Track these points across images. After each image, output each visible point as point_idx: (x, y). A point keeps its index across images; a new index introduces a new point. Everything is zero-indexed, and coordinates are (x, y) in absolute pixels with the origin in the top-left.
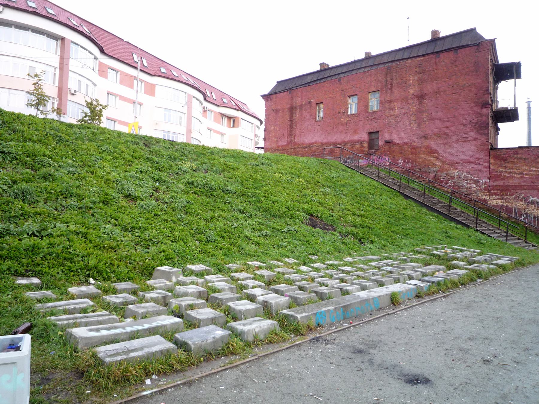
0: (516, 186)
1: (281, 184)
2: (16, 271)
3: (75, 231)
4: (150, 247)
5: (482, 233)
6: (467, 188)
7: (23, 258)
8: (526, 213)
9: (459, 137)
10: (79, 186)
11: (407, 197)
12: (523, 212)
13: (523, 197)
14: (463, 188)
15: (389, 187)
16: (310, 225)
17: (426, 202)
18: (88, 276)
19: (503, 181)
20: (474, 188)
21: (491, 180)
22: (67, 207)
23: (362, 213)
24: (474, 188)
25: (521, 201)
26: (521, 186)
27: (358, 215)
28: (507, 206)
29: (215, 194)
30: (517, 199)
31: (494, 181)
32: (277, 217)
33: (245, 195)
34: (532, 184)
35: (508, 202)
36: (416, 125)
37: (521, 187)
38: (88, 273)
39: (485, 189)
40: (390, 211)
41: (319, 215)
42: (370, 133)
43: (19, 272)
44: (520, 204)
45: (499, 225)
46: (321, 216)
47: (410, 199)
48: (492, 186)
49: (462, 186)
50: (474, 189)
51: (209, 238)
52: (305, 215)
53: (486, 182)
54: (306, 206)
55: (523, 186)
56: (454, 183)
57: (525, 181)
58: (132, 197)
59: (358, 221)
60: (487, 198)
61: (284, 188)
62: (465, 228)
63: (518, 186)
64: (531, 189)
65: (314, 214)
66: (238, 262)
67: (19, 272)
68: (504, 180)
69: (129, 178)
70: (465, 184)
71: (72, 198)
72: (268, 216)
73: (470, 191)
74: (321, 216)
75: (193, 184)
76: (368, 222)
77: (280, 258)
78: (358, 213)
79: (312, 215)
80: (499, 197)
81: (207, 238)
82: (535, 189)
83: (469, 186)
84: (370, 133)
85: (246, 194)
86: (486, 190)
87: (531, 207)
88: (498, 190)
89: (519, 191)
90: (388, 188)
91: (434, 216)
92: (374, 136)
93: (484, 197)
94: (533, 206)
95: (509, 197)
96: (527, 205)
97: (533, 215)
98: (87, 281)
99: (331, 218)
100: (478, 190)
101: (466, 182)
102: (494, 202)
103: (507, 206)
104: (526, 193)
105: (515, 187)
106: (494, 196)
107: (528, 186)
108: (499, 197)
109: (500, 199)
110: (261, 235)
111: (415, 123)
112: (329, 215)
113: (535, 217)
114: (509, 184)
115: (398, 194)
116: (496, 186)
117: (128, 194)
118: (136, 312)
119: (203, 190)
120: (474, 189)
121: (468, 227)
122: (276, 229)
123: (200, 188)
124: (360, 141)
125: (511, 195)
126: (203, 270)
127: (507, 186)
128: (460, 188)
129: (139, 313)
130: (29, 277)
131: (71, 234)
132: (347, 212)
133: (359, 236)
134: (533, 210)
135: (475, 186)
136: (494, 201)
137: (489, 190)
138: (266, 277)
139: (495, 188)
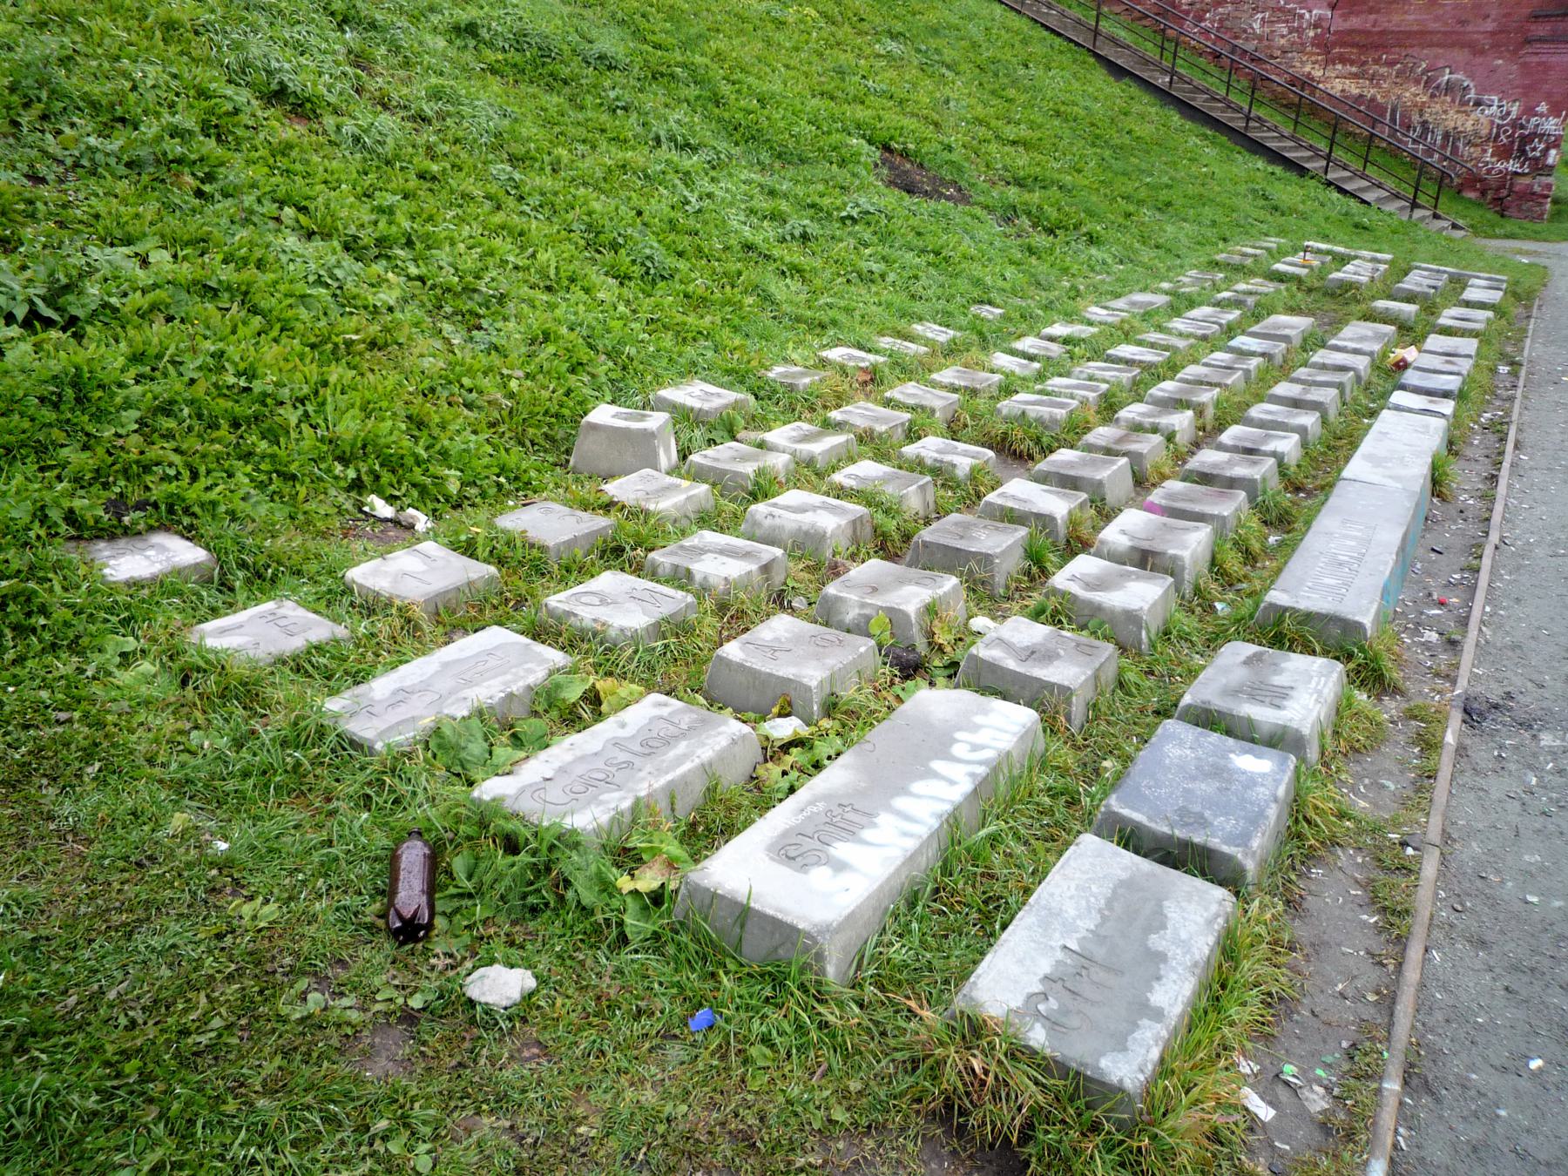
0: (1409, 34)
1: (751, 27)
2: (71, 517)
3: (195, 282)
4: (484, 323)
5: (1341, 191)
6: (1260, 38)
7: (62, 446)
8: (1424, 123)
10: (69, 58)
11: (1118, 71)
12: (1416, 118)
13: (1425, 72)
14: (1247, 39)
15: (1059, 35)
16: (896, 185)
17: (1178, 90)
18: (357, 485)
19: (1373, 17)
20: (1283, 36)
21: (1338, 12)
22: (76, 165)
23: (1023, 132)
24: (1283, 36)
25: (1417, 82)
26: (1422, 33)
27: (1014, 143)
28: (1373, 99)
29: (565, 72)
30: (1405, 76)
31: (1345, 17)
32: (796, 160)
33: (662, 75)
34: (1458, 28)
35: (1378, 86)
37: (1421, 37)
38: (351, 474)
39: (1319, 42)
40: (1093, 125)
41: (911, 146)
43: (91, 522)
44: (1412, 94)
45: (1366, 161)
46: (917, 152)
47: (1127, 80)
48: (1336, 32)
49: (1245, 31)
50: (1283, 41)
51: (649, 264)
52: (866, 147)
53: (1320, 18)
54: (861, 113)
55: (1431, 33)
56: (1221, 21)
57: (1437, 19)
58: (292, 100)
59: (1022, 161)
60: (1318, 73)
61: (768, 42)
62: (1293, 176)
63: (1416, 33)
64: (1453, 45)
65: (894, 145)
66: (795, 356)
67: (91, 522)
68: (1378, 12)
69: (245, 14)
70: (1256, 26)
71: (75, 119)
72: (765, 157)
73: (1269, 47)
74: (917, 152)
75: (475, 35)
76: (1053, 167)
77: (902, 325)
78: (1010, 132)
79: (887, 148)
80: (1354, 69)
81: (643, 264)
82: (1463, 46)
83: (1267, 30)
85: (663, 69)
86: (1318, 46)
87: (1443, 103)
88: (1352, 45)
89: (1415, 51)
90: (1058, 40)
91: (1206, 137)
93: (1307, 69)
94: (1448, 99)
95: (1384, 70)
96: (1433, 96)
97: (1441, 128)
98: (359, 506)
99: (946, 155)
100: (1293, 43)
101: (1260, 16)
102: (1337, 86)
103: (1373, 99)
104: (1436, 57)
105: (1405, 39)
106: (1339, 67)
107: (1445, 33)
108: (1354, 69)
109: (1355, 76)
110: (788, 238)
112: (940, 147)
113: (1446, 136)
114: (1390, 27)
115: (1092, 60)
116: (1351, 32)
117: (274, 86)
118: (786, 681)
119: (518, 58)
120: (1283, 41)
121: (1302, 171)
122: (821, 210)
123: (504, 50)
125: (1391, 64)
126: (726, 406)
127: (1382, 33)
128: (1236, 38)
129: (808, 689)
130: (139, 533)
131: (184, 296)
132: (982, 132)
133: (1047, 219)
134: (1445, 112)
135: (1285, 31)
136: (1338, 83)
137: (1329, 47)
138: (938, 414)
139: (1345, 38)
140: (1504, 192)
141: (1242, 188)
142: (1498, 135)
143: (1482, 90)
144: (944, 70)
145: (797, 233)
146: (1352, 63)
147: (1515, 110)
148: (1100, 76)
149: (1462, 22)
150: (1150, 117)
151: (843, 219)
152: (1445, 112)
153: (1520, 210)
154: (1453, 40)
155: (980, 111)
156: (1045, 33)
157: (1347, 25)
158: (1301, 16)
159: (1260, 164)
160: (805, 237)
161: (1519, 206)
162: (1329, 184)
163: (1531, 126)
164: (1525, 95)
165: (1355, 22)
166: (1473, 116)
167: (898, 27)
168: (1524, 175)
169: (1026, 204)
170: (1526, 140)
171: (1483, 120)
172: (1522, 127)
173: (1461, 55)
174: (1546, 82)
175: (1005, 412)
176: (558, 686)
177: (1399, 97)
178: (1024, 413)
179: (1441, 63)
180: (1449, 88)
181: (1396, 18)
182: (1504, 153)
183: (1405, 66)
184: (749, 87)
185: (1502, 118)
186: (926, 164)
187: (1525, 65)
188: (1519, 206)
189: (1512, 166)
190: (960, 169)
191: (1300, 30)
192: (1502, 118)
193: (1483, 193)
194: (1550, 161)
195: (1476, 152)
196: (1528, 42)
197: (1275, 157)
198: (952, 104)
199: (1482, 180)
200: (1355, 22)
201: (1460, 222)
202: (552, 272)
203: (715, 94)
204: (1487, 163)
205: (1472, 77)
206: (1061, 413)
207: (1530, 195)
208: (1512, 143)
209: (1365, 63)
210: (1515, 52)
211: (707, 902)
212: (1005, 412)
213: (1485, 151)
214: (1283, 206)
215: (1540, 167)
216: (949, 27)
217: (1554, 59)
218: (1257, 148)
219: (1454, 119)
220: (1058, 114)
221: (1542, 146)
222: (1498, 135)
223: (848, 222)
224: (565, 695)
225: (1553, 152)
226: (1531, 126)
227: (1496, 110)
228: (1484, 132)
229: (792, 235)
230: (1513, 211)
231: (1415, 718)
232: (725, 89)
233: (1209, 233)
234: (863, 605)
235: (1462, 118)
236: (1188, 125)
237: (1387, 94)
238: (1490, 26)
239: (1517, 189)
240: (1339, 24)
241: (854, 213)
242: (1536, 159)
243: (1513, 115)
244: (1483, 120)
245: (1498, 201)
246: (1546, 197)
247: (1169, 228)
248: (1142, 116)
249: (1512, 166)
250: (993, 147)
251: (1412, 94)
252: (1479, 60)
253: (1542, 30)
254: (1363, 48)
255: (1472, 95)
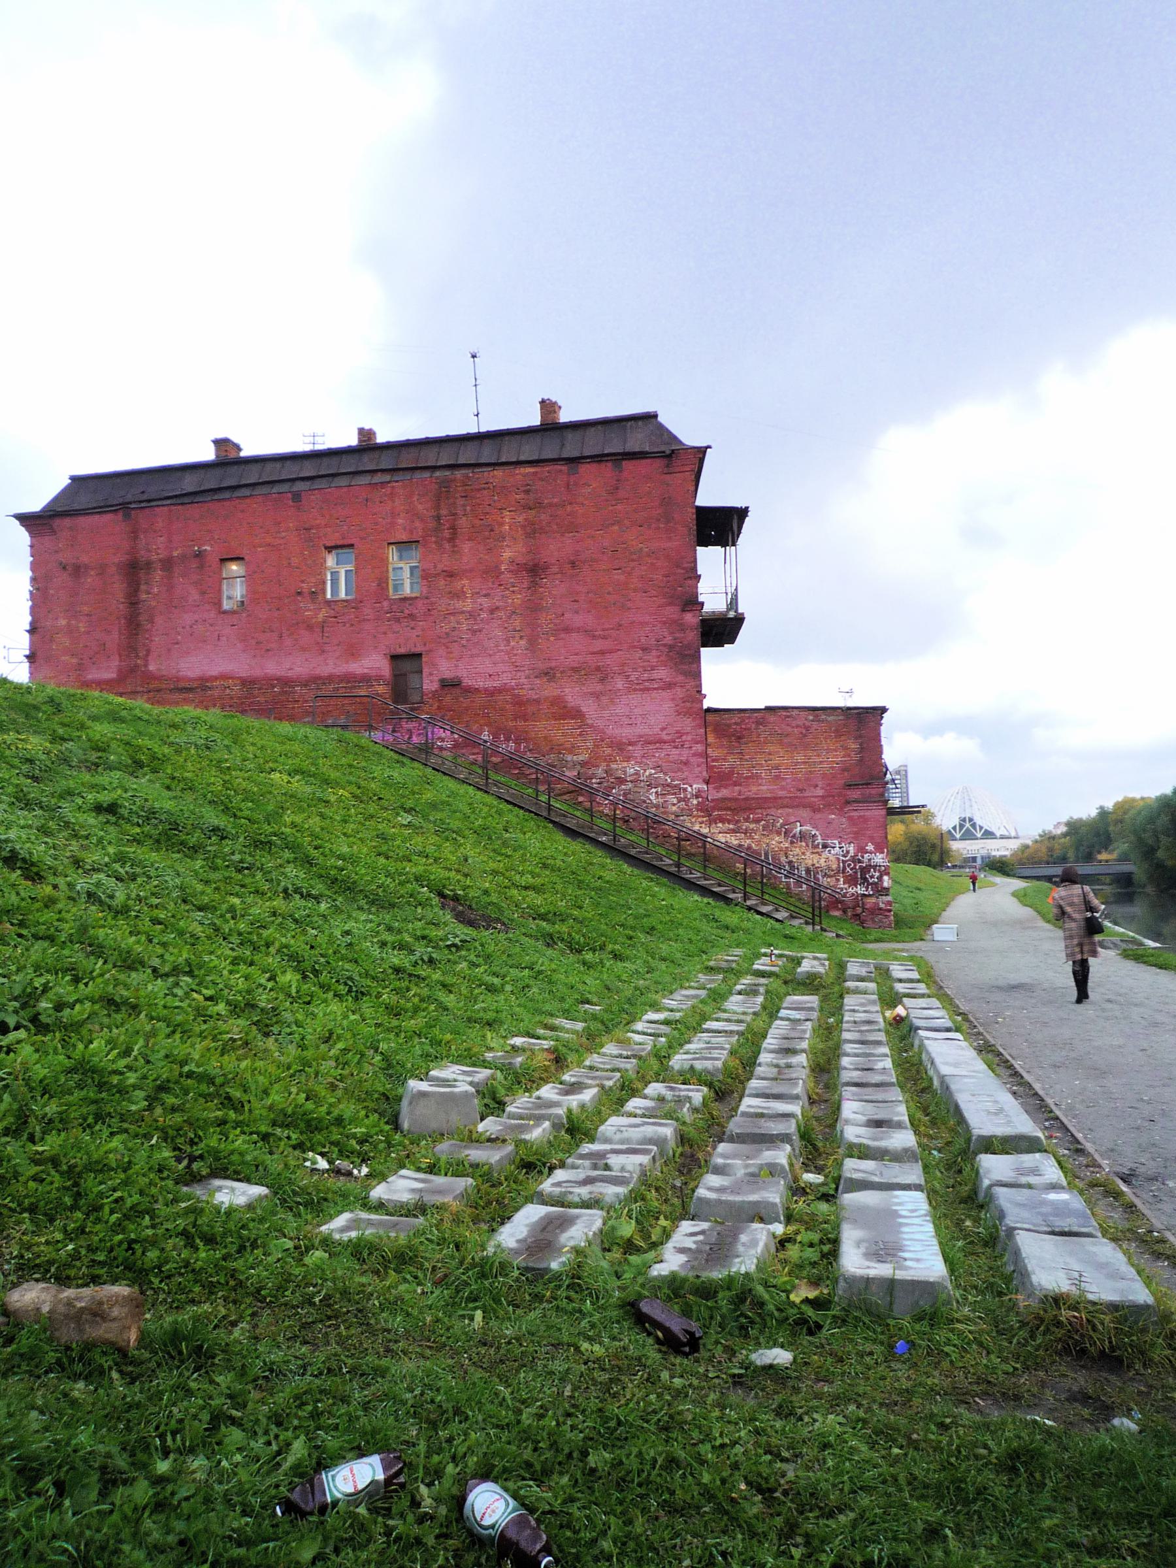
6: (657, 806)
8: (790, 863)
9: (632, 678)
12: (783, 859)
13: (783, 825)
19: (737, 788)
25: (779, 833)
28: (749, 848)
30: (769, 829)
31: (718, 789)
33: (262, 843)
34: (799, 794)
36: (522, 642)
39: (701, 808)
42: (395, 658)
44: (776, 842)
48: (713, 800)
49: (644, 802)
50: (674, 808)
57: (783, 788)
60: (705, 831)
62: (721, 904)
64: (797, 806)
68: (740, 785)
70: (653, 797)
80: (731, 826)
81: (346, 984)
82: (805, 806)
84: (395, 658)
85: (262, 838)
86: (701, 810)
87: (801, 847)
88: (729, 809)
89: (772, 811)
91: (652, 880)
92: (407, 666)
95: (752, 826)
96: (792, 842)
100: (683, 809)
101: (654, 790)
103: (749, 848)
104: (788, 815)
105: (764, 803)
106: (720, 825)
108: (731, 826)
109: (733, 831)
111: (521, 637)
115: (551, 825)
116: (724, 799)
120: (674, 808)
124: (365, 679)
125: (757, 821)
129: (775, 1205)
134: (803, 853)
135: (675, 801)
137: (709, 811)
139: (720, 804)
140: (859, 910)
141: (696, 914)
142: (844, 868)
143: (825, 836)
144: (454, 836)
145: (426, 958)
146: (729, 822)
147: (852, 849)
148: (559, 836)
149: (801, 790)
150: (612, 869)
151: (448, 946)
152: (803, 853)
153: (874, 922)
154: (796, 802)
155: (492, 865)
156: (510, 807)
157: (720, 795)
158: (685, 790)
159: (696, 897)
160: (431, 961)
161: (872, 919)
162: (749, 909)
163: (865, 860)
164: (856, 838)
165: (724, 793)
166: (824, 855)
167: (409, 804)
168: (869, 896)
169: (559, 932)
170: (865, 870)
171: (832, 858)
172: (860, 861)
173: (805, 813)
174: (867, 829)
175: (677, 1067)
176: (613, 1228)
177: (768, 845)
178: (692, 1067)
179: (792, 819)
180: (803, 836)
181: (754, 789)
182: (852, 881)
183: (767, 821)
184: (331, 850)
185: (844, 856)
186: (474, 906)
187: (850, 819)
188: (872, 919)
189: (860, 890)
190: (500, 909)
191: (686, 800)
192: (844, 856)
193: (845, 912)
194: (886, 884)
195: (832, 881)
196: (848, 802)
197: (705, 891)
198: (470, 861)
199: (842, 902)
200: (724, 793)
201: (841, 933)
202: (293, 991)
203: (307, 856)
204: (842, 889)
205: (816, 827)
206: (719, 1064)
207: (876, 911)
208: (856, 873)
209: (738, 822)
210: (841, 809)
211: (862, 1286)
212: (677, 1067)
213: (838, 880)
214: (732, 926)
215: (881, 891)
216: (443, 803)
217: (868, 813)
218: (691, 885)
219: (810, 859)
220: (545, 866)
221: (877, 874)
222: (844, 868)
223: (453, 949)
224: (619, 1233)
225: (886, 878)
226: (865, 860)
227: (836, 853)
228: (834, 867)
229: (422, 960)
230: (869, 924)
231: (1096, 1185)
232: (314, 853)
233: (692, 948)
234: (747, 1166)
235: (816, 857)
236: (636, 872)
237: (759, 842)
238: (820, 792)
239: (867, 906)
240: (714, 795)
241: (457, 941)
242: (876, 884)
243: (852, 853)
244: (832, 858)
245: (857, 916)
246: (890, 911)
247: (664, 947)
248: (603, 866)
249: (860, 890)
250: (515, 892)
251: (776, 842)
252: (818, 816)
253: (855, 794)
254: (735, 811)
255: (819, 840)
